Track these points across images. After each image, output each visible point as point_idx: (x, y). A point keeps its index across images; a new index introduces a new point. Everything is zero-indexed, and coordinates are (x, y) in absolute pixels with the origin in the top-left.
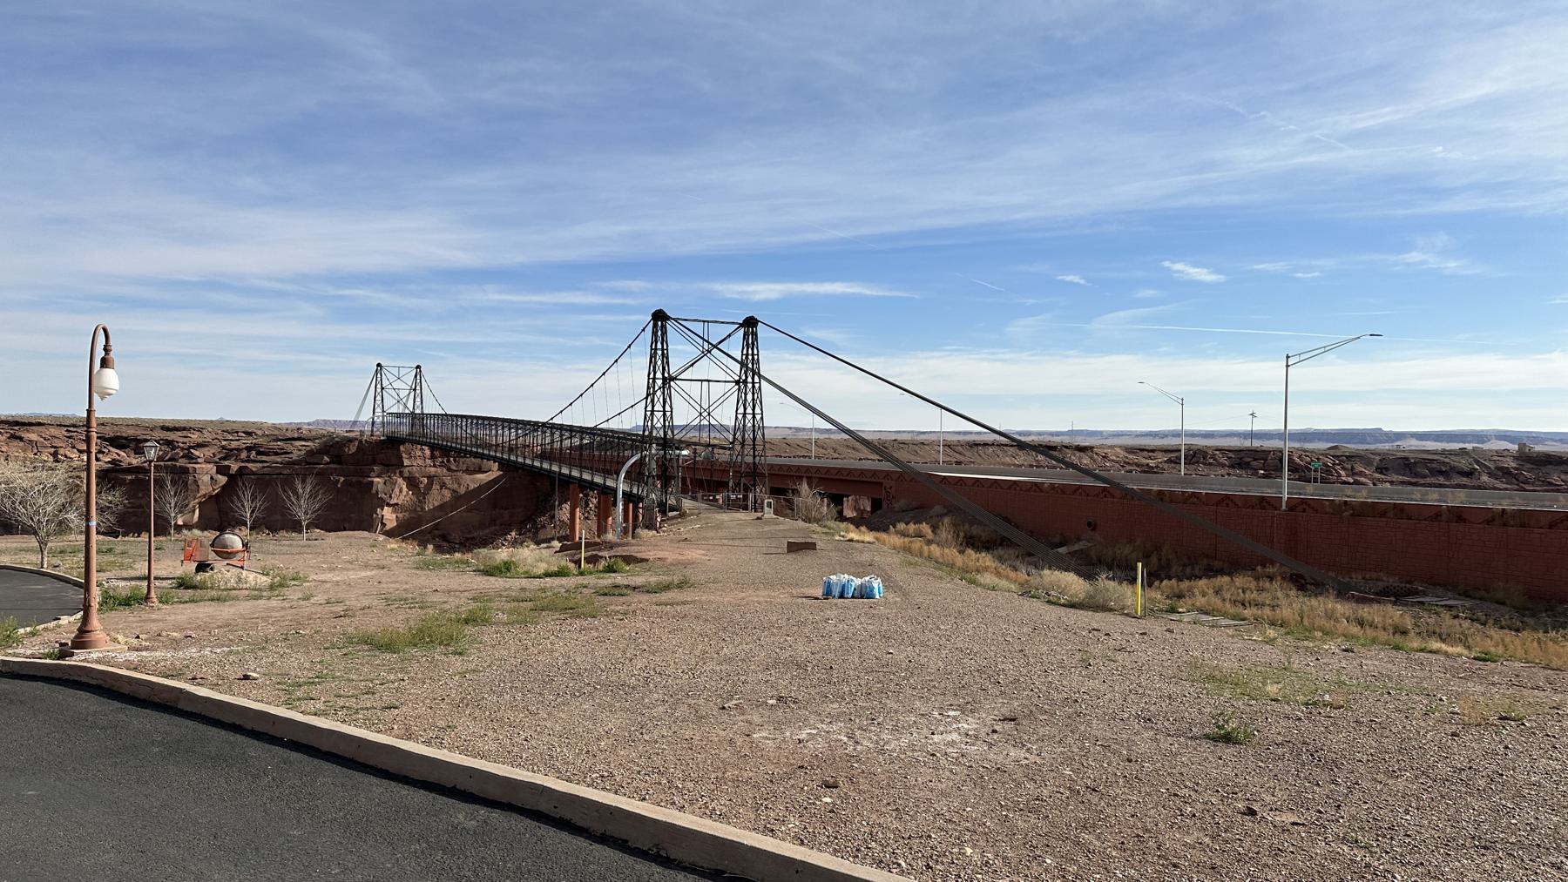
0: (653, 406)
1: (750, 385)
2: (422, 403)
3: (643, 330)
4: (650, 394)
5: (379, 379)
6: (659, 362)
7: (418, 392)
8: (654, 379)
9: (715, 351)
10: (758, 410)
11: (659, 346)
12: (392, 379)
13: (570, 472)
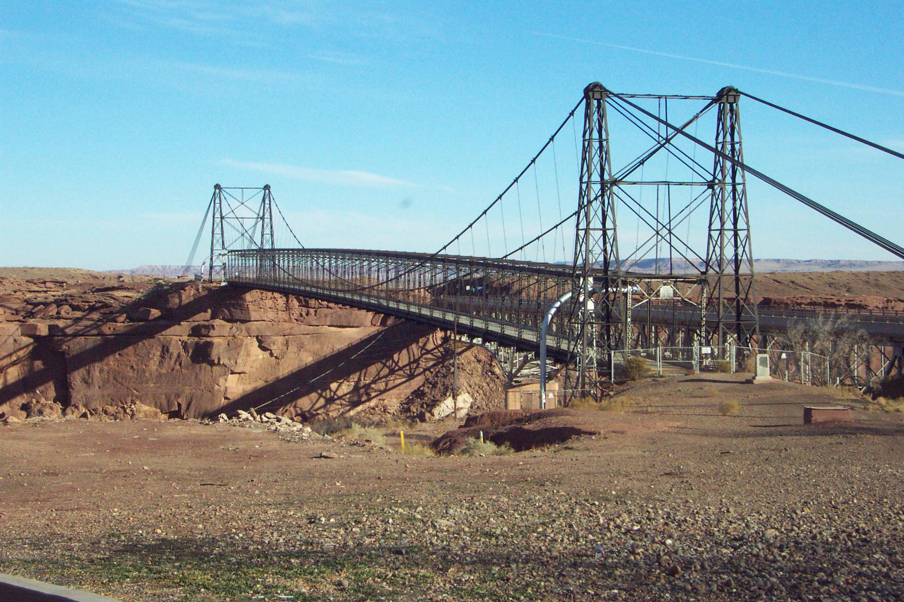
0: (588, 224)
1: (729, 188)
2: (272, 235)
3: (572, 114)
4: (583, 206)
5: (218, 205)
7: (267, 221)
9: (679, 141)
10: (741, 224)
11: (595, 135)
12: (234, 204)
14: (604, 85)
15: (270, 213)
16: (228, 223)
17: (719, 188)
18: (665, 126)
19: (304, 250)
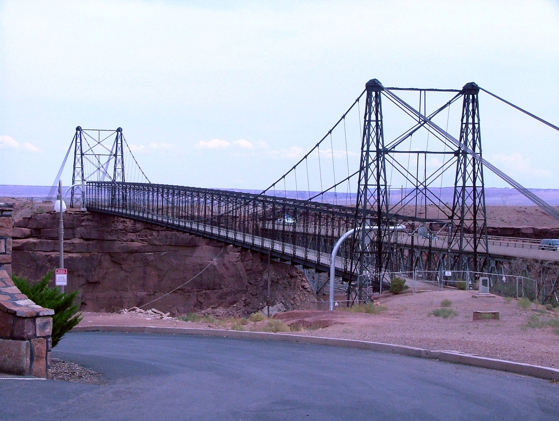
0: (366, 181)
2: (123, 170)
3: (358, 100)
5: (79, 144)
6: (373, 135)
7: (119, 157)
8: (368, 151)
11: (373, 117)
13: (283, 248)
14: (378, 80)
15: (122, 151)
16: (87, 158)
17: (463, 156)
18: (421, 113)
19: (150, 185)
